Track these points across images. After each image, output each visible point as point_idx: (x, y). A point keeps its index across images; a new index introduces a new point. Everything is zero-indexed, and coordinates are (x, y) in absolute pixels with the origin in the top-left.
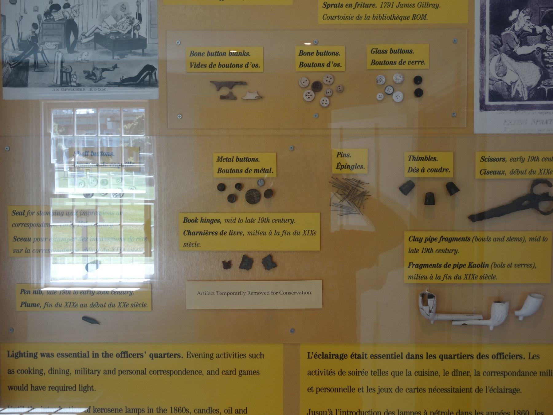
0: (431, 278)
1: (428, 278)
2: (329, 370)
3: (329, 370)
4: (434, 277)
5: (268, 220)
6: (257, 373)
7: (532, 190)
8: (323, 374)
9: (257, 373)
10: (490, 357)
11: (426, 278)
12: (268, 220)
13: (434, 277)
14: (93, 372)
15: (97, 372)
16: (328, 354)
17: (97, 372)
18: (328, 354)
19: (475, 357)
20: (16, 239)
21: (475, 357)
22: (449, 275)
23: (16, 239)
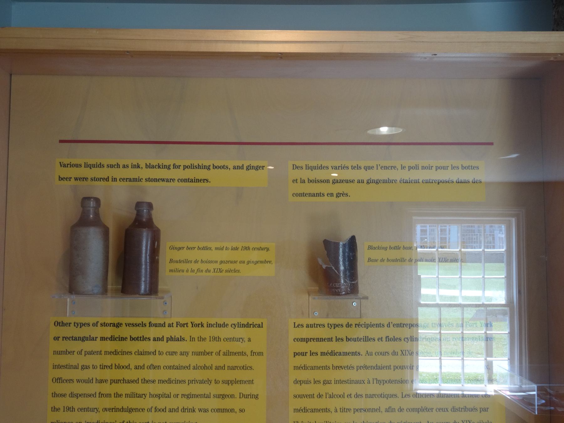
0: (187, 271)
1: (185, 271)
2: (349, 365)
3: (349, 365)
4: (190, 271)
5: (249, 248)
6: (61, 141)
7: (97, 294)
8: (410, 340)
9: (61, 141)
10: (91, 325)
11: (183, 271)
12: (249, 248)
13: (190, 271)
14: (140, 396)
15: (143, 396)
16: (193, 179)
17: (143, 396)
18: (193, 179)
19: (344, 326)
20: (171, 261)
21: (344, 326)
22: (201, 269)
23: (171, 261)
